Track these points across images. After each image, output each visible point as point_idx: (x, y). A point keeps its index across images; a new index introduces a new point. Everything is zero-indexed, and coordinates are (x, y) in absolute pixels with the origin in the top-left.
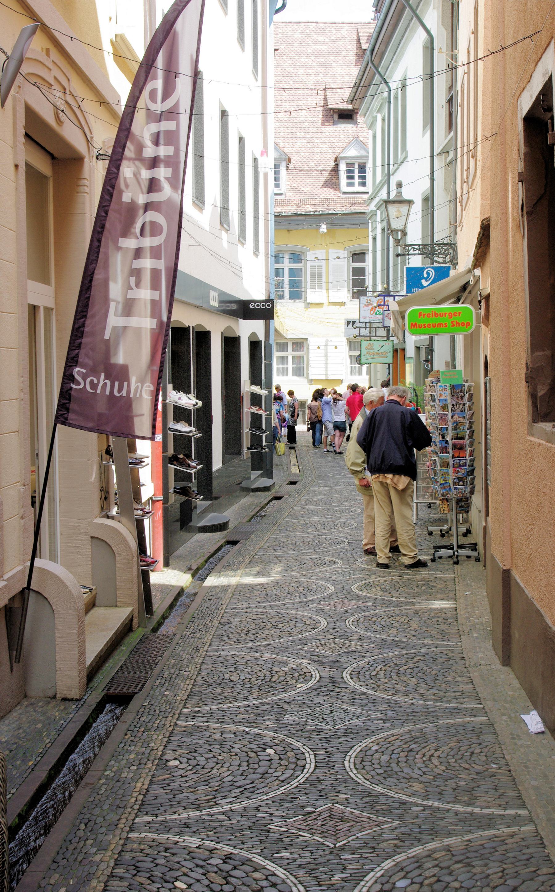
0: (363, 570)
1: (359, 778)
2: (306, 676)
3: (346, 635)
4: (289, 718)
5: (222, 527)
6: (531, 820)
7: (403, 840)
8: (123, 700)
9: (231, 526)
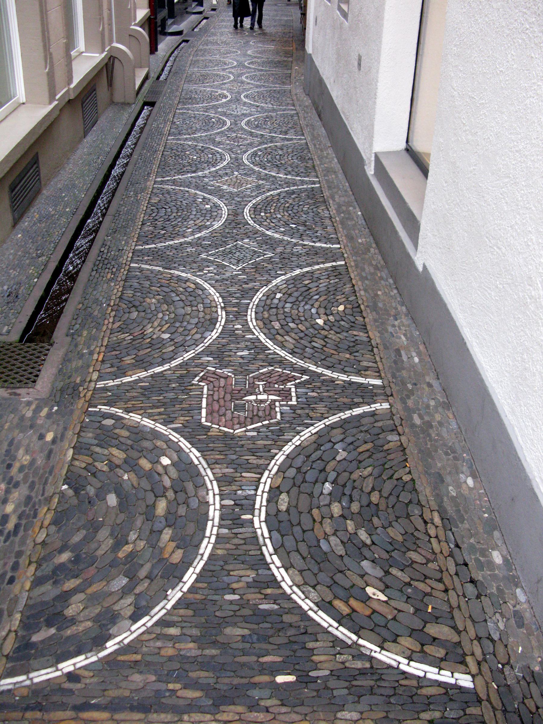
0: (251, 56)
1: (247, 128)
2: (226, 97)
3: (242, 82)
4: (219, 110)
5: (180, 33)
6: (320, 183)
7: (260, 144)
8: (152, 104)
9: (184, 33)
